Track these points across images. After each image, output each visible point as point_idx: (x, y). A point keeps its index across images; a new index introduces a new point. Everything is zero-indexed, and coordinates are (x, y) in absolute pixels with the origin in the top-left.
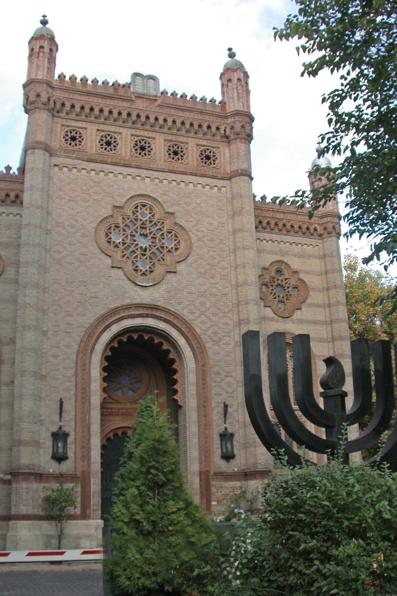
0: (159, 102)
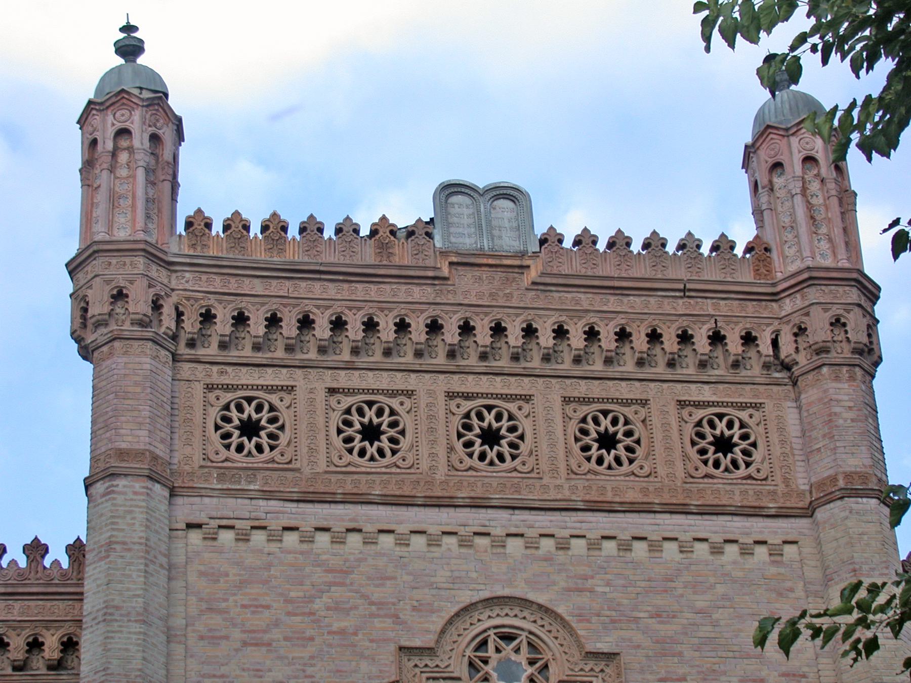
0: (533, 274)
